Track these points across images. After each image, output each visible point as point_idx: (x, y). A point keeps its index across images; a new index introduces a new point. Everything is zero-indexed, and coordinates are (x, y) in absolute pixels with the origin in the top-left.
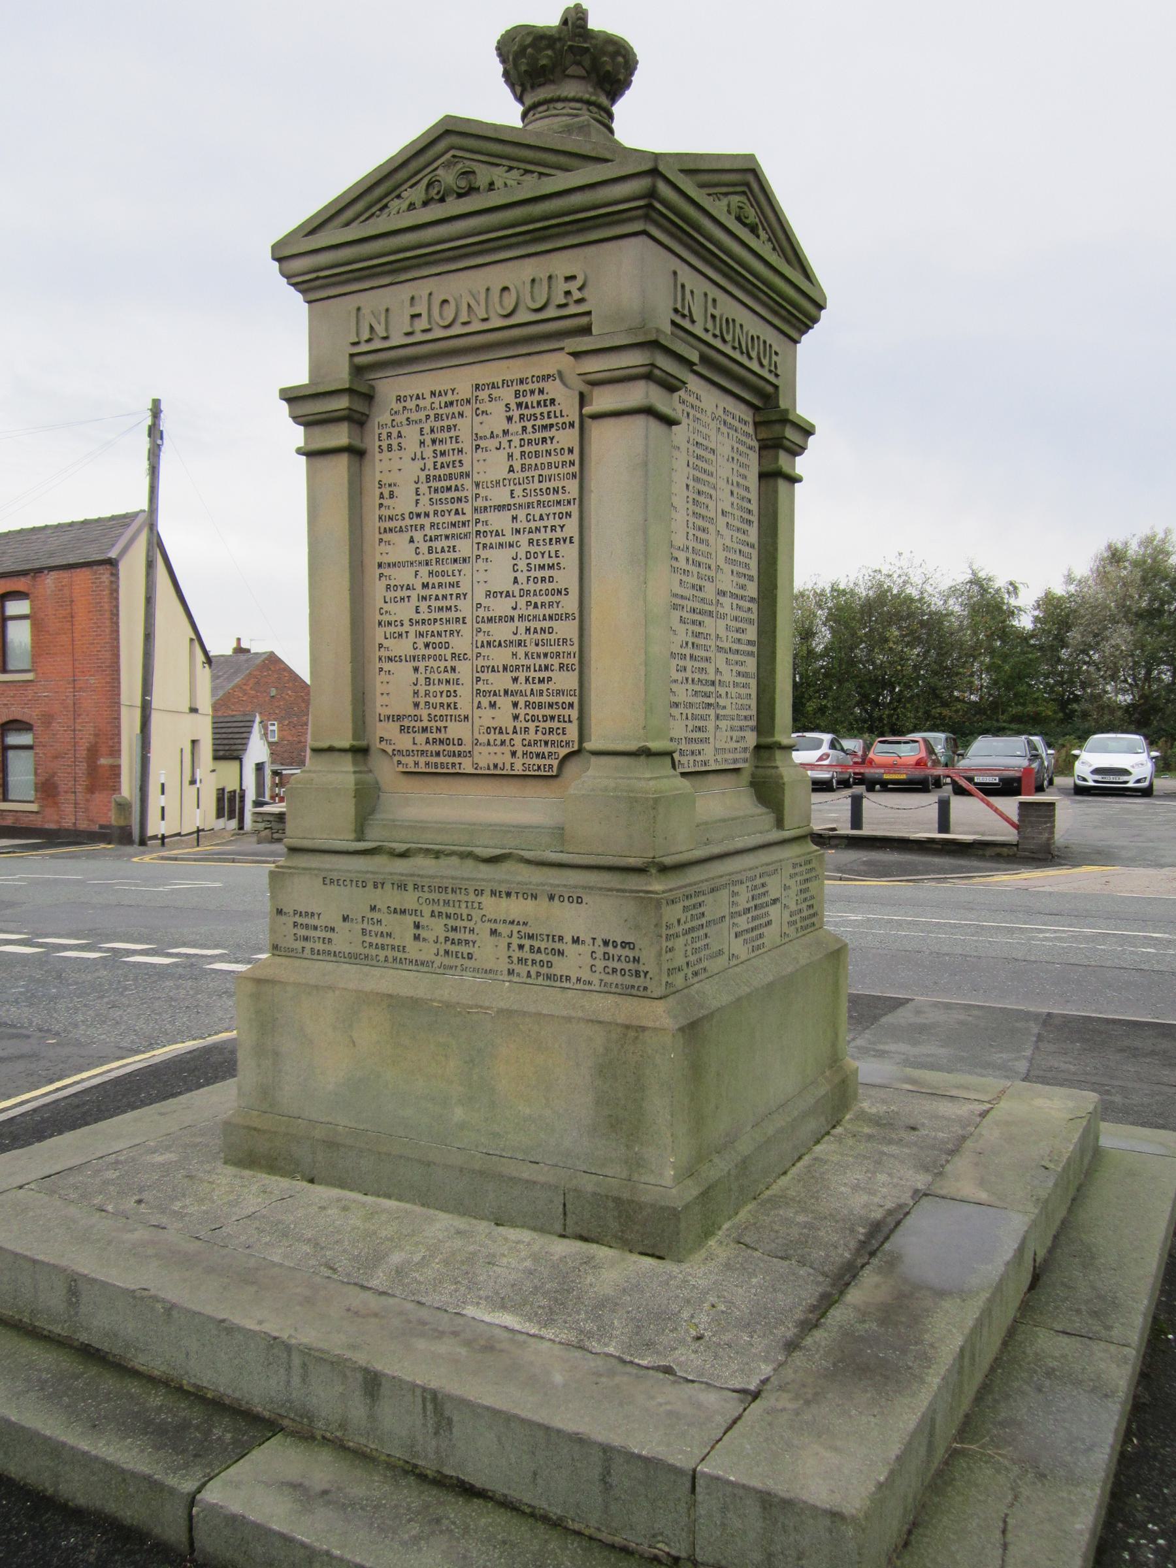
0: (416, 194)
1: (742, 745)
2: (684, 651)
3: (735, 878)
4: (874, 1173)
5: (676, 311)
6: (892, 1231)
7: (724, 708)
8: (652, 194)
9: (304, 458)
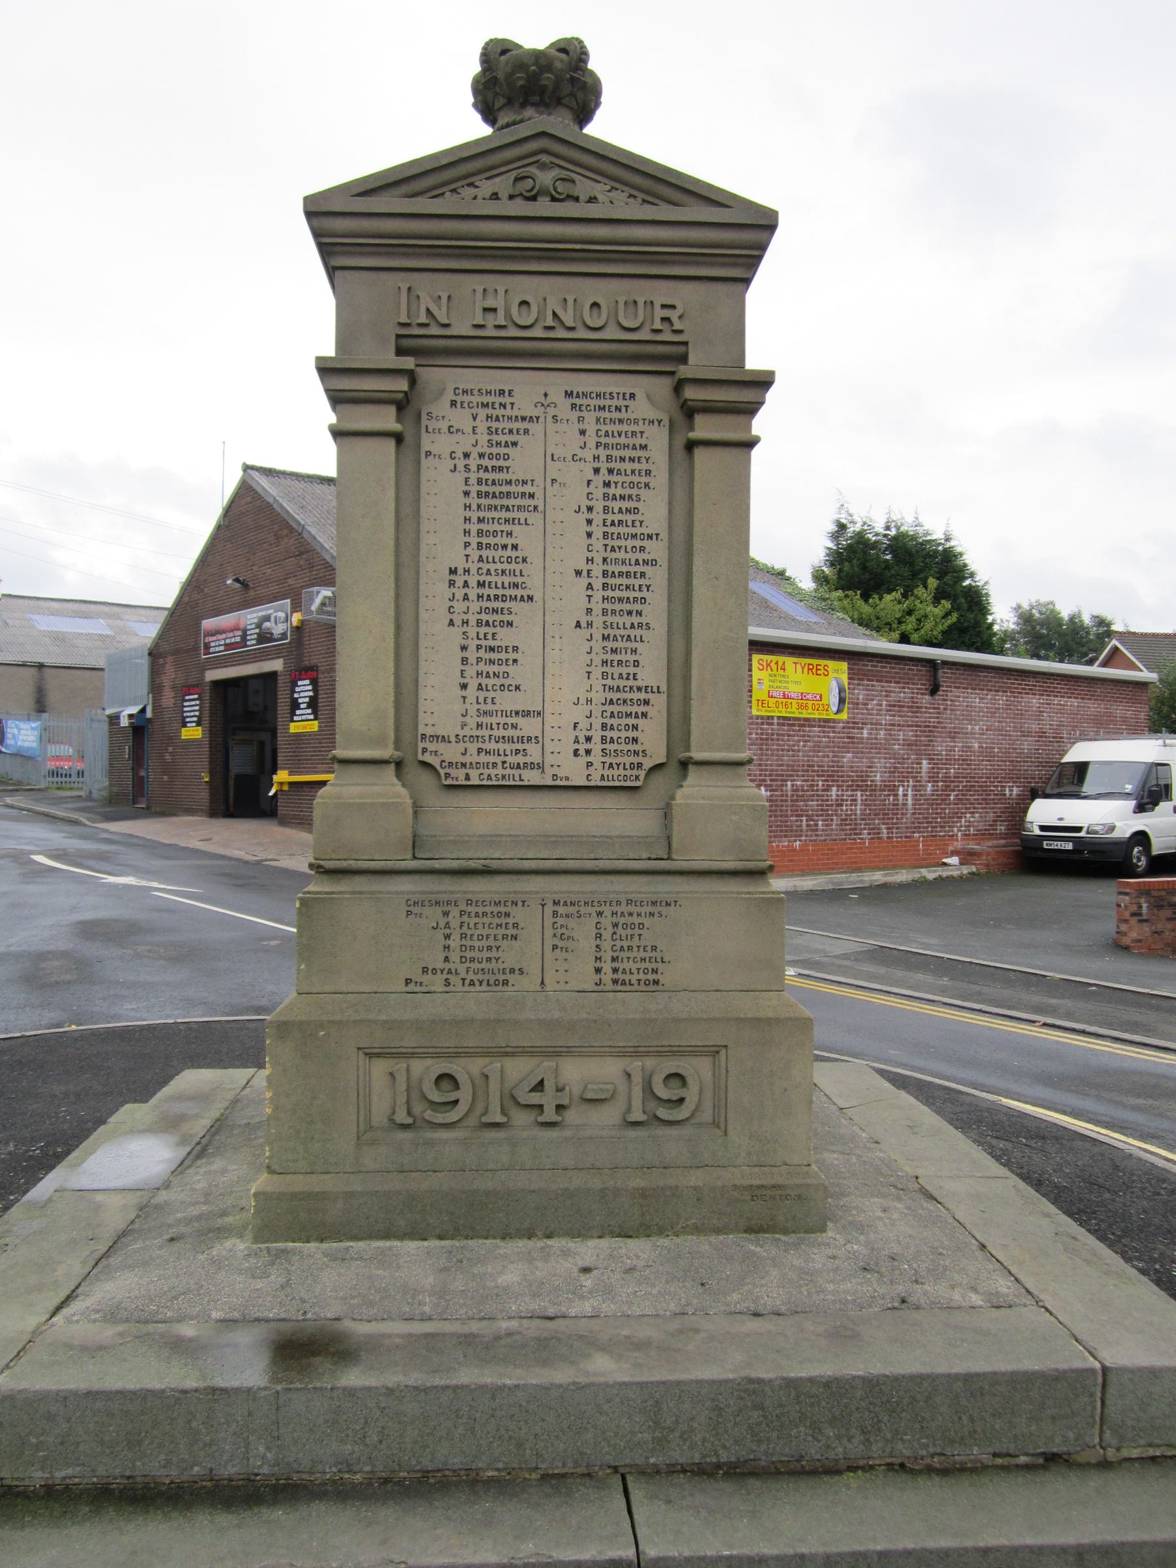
0: (503, 184)
4: (210, 1186)
6: (186, 1158)
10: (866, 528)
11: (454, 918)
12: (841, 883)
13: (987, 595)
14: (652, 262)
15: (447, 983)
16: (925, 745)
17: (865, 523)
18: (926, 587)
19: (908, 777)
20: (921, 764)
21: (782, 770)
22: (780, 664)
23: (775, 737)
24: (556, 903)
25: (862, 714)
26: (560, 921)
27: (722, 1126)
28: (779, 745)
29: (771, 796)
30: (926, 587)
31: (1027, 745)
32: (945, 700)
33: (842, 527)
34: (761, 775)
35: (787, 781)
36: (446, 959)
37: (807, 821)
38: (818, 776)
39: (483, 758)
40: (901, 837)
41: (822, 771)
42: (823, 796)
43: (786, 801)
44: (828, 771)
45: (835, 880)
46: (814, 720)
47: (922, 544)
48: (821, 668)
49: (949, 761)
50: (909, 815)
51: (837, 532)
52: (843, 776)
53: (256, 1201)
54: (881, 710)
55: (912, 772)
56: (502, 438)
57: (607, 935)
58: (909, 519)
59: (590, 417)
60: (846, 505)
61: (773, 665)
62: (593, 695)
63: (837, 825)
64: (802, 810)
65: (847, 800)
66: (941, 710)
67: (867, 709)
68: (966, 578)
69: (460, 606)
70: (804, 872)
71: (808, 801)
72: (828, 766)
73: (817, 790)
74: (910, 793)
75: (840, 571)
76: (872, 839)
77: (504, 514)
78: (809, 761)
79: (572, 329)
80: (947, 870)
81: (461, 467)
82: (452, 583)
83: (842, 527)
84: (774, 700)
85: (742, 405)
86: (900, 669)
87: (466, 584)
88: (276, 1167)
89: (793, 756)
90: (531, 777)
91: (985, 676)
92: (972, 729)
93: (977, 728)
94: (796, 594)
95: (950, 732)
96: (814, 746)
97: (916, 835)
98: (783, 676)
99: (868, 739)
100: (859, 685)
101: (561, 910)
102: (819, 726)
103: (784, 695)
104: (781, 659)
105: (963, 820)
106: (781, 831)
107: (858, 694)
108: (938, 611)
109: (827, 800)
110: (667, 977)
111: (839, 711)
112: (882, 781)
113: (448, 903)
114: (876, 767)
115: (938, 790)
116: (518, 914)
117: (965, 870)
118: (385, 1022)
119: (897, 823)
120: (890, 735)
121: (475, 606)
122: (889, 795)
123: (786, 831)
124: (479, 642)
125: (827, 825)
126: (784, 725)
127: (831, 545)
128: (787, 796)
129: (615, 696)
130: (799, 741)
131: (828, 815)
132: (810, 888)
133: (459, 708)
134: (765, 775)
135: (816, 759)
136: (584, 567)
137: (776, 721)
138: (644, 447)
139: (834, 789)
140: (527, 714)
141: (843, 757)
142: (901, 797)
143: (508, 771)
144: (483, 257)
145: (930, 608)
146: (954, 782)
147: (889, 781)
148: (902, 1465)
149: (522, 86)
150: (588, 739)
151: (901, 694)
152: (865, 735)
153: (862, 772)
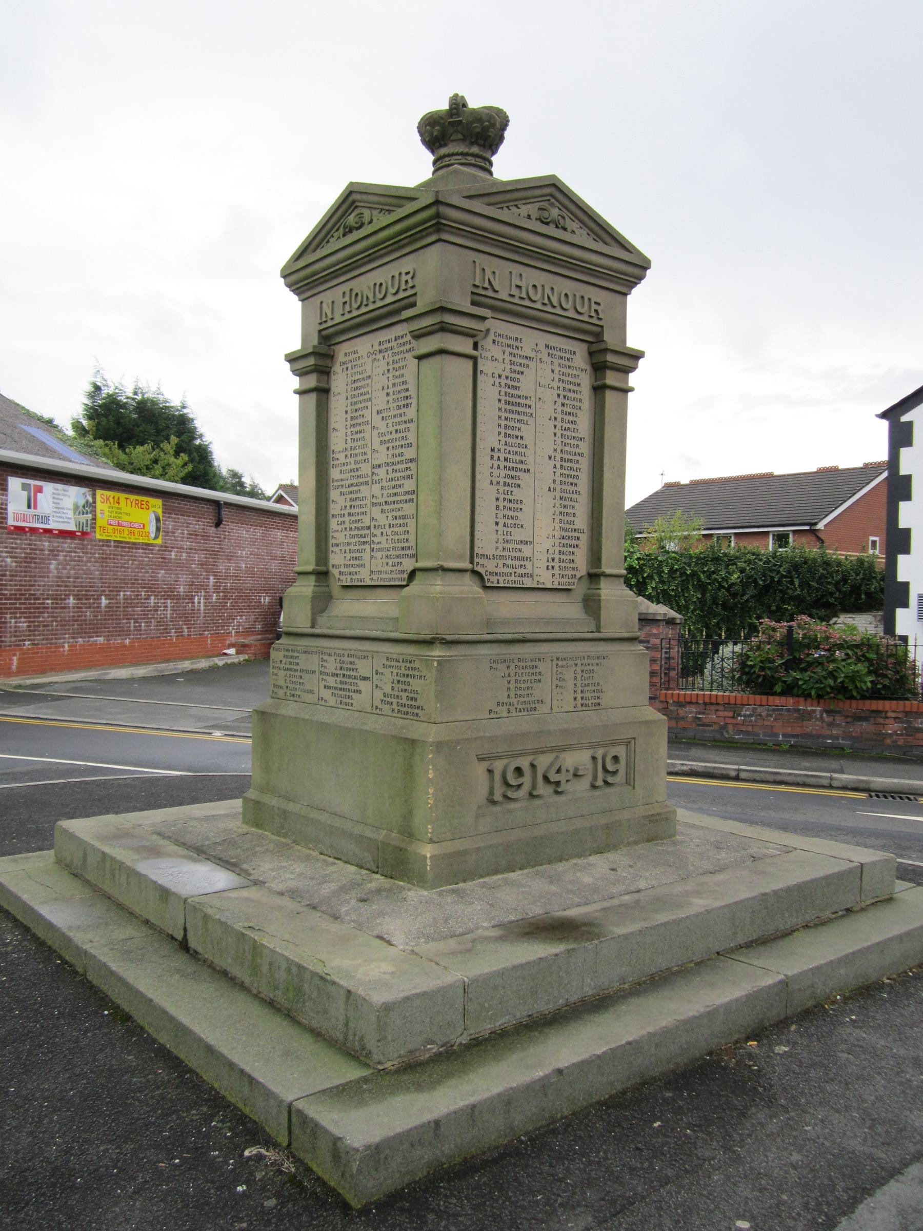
1: (399, 568)
2: (343, 512)
3: (325, 650)
5: (475, 286)
7: (379, 543)
8: (438, 215)
9: (298, 396)
10: (117, 391)
11: (512, 670)
12: (163, 671)
13: (211, 453)
14: (592, 275)
15: (509, 712)
16: (212, 565)
17: (116, 388)
18: (169, 443)
19: (201, 589)
20: (209, 579)
21: (117, 583)
22: (116, 499)
23: (112, 556)
24: (558, 659)
25: (171, 540)
26: (560, 670)
27: (632, 784)
28: (115, 563)
29: (109, 603)
30: (169, 443)
31: (274, 566)
32: (224, 531)
33: (97, 388)
34: (102, 587)
35: (120, 591)
36: (509, 696)
37: (134, 623)
38: (142, 587)
39: (506, 570)
40: (196, 635)
41: (145, 584)
42: (145, 603)
43: (120, 607)
44: (148, 584)
45: (159, 669)
46: (139, 544)
47: (162, 409)
48: (144, 503)
49: (227, 577)
50: (201, 618)
51: (94, 392)
52: (158, 588)
53: (431, 862)
54: (183, 538)
55: (203, 585)
56: (517, 368)
57: (579, 678)
58: (153, 388)
59: (556, 362)
60: (101, 372)
61: (111, 500)
62: (555, 533)
63: (154, 626)
64: (130, 615)
65: (161, 607)
66: (222, 539)
67: (174, 537)
68: (196, 439)
69: (496, 472)
70: (135, 663)
71: (134, 607)
72: (149, 580)
73: (141, 599)
74: (202, 601)
75: (99, 424)
76: (178, 636)
77: (517, 417)
78: (135, 576)
79: (554, 307)
80: (230, 659)
81: (497, 384)
82: (492, 457)
83: (97, 388)
84: (112, 527)
85: (617, 366)
86: (196, 506)
87: (499, 459)
88: (435, 839)
89: (125, 572)
90: (528, 583)
91: (249, 515)
92: (241, 553)
93: (244, 552)
94: (64, 439)
95: (228, 556)
96: (139, 564)
97: (206, 633)
98: (118, 508)
99: (175, 559)
100: (169, 517)
101: (560, 663)
102: (143, 549)
103: (119, 523)
104: (117, 495)
105: (235, 621)
106: (116, 631)
107: (169, 525)
108: (179, 462)
109: (148, 607)
110: (606, 700)
111: (156, 537)
112: (185, 592)
113: (510, 661)
114: (180, 581)
115: (219, 599)
116: (542, 667)
117: (242, 658)
118: (490, 737)
119: (194, 624)
120: (189, 557)
121: (503, 473)
122: (188, 603)
123: (120, 631)
124: (505, 496)
125: (147, 626)
126: (118, 547)
127: (88, 402)
128: (120, 603)
129: (565, 534)
130: (129, 560)
131: (148, 618)
132: (142, 675)
133: (494, 537)
134: (105, 587)
135: (140, 574)
136: (552, 454)
137: (112, 544)
138: (579, 385)
139: (153, 598)
140: (526, 543)
141: (158, 573)
142: (196, 604)
143: (518, 579)
144: (517, 252)
145: (173, 459)
146: (229, 593)
147: (189, 592)
148: (807, 926)
149: (478, 133)
150: (553, 559)
151: (197, 526)
152: (173, 557)
153: (171, 585)
